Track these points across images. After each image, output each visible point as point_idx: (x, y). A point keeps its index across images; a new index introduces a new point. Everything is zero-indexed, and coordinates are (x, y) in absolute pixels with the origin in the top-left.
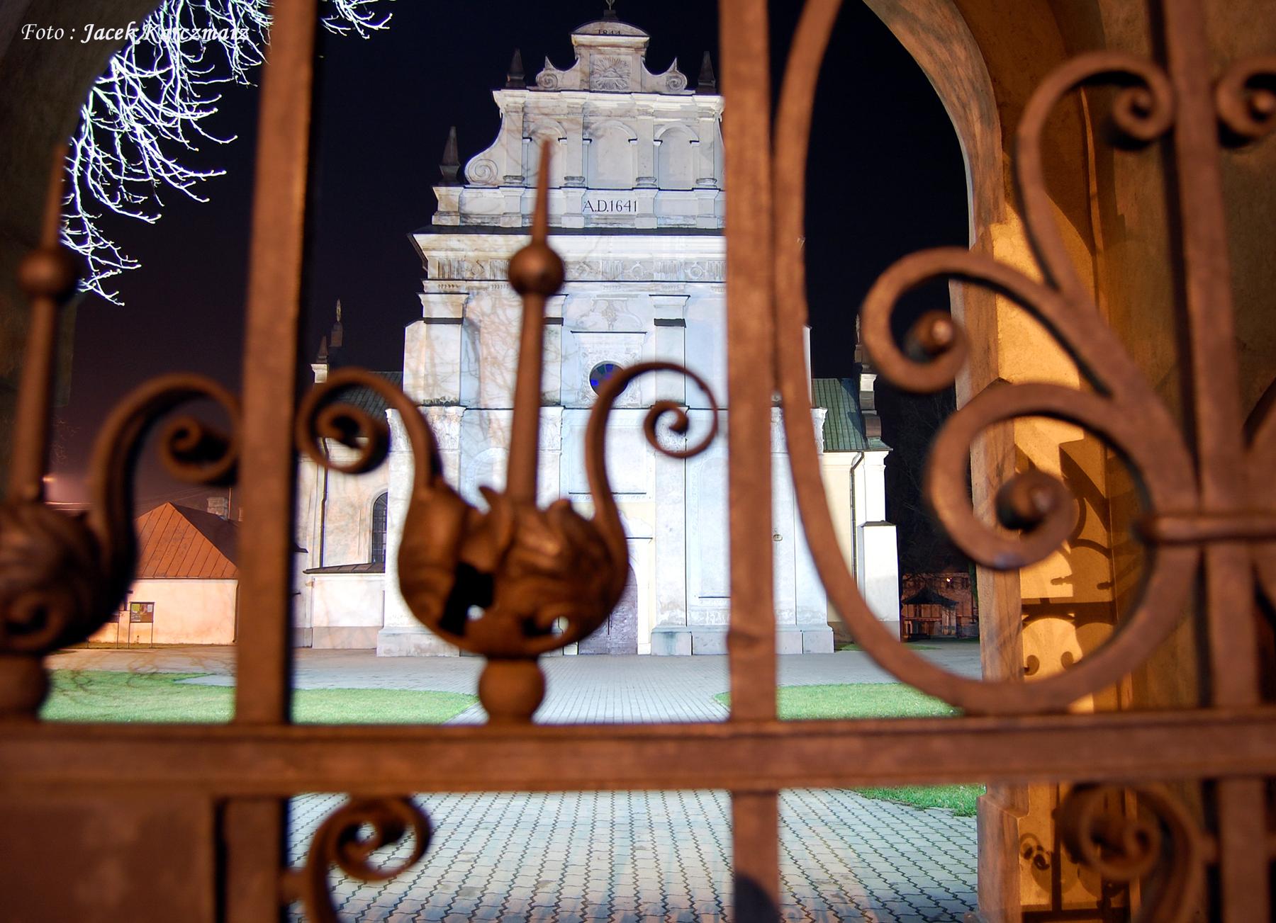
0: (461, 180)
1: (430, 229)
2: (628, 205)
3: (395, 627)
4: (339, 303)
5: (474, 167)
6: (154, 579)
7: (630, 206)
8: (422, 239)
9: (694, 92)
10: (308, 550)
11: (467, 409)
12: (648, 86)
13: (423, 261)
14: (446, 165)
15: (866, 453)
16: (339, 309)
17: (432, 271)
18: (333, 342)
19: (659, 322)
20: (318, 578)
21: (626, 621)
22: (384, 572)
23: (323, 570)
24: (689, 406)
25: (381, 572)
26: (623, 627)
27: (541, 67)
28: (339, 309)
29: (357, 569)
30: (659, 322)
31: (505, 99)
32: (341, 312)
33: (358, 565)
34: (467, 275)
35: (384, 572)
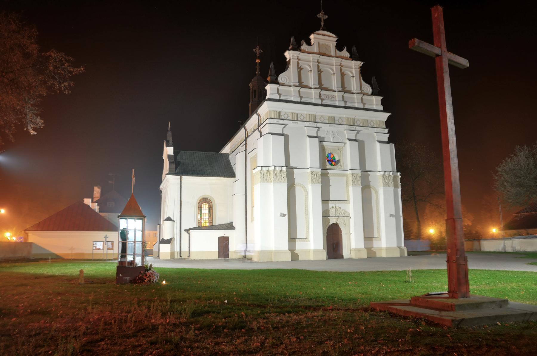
5: (282, 78)
10: (175, 221)
12: (337, 55)
31: (289, 55)
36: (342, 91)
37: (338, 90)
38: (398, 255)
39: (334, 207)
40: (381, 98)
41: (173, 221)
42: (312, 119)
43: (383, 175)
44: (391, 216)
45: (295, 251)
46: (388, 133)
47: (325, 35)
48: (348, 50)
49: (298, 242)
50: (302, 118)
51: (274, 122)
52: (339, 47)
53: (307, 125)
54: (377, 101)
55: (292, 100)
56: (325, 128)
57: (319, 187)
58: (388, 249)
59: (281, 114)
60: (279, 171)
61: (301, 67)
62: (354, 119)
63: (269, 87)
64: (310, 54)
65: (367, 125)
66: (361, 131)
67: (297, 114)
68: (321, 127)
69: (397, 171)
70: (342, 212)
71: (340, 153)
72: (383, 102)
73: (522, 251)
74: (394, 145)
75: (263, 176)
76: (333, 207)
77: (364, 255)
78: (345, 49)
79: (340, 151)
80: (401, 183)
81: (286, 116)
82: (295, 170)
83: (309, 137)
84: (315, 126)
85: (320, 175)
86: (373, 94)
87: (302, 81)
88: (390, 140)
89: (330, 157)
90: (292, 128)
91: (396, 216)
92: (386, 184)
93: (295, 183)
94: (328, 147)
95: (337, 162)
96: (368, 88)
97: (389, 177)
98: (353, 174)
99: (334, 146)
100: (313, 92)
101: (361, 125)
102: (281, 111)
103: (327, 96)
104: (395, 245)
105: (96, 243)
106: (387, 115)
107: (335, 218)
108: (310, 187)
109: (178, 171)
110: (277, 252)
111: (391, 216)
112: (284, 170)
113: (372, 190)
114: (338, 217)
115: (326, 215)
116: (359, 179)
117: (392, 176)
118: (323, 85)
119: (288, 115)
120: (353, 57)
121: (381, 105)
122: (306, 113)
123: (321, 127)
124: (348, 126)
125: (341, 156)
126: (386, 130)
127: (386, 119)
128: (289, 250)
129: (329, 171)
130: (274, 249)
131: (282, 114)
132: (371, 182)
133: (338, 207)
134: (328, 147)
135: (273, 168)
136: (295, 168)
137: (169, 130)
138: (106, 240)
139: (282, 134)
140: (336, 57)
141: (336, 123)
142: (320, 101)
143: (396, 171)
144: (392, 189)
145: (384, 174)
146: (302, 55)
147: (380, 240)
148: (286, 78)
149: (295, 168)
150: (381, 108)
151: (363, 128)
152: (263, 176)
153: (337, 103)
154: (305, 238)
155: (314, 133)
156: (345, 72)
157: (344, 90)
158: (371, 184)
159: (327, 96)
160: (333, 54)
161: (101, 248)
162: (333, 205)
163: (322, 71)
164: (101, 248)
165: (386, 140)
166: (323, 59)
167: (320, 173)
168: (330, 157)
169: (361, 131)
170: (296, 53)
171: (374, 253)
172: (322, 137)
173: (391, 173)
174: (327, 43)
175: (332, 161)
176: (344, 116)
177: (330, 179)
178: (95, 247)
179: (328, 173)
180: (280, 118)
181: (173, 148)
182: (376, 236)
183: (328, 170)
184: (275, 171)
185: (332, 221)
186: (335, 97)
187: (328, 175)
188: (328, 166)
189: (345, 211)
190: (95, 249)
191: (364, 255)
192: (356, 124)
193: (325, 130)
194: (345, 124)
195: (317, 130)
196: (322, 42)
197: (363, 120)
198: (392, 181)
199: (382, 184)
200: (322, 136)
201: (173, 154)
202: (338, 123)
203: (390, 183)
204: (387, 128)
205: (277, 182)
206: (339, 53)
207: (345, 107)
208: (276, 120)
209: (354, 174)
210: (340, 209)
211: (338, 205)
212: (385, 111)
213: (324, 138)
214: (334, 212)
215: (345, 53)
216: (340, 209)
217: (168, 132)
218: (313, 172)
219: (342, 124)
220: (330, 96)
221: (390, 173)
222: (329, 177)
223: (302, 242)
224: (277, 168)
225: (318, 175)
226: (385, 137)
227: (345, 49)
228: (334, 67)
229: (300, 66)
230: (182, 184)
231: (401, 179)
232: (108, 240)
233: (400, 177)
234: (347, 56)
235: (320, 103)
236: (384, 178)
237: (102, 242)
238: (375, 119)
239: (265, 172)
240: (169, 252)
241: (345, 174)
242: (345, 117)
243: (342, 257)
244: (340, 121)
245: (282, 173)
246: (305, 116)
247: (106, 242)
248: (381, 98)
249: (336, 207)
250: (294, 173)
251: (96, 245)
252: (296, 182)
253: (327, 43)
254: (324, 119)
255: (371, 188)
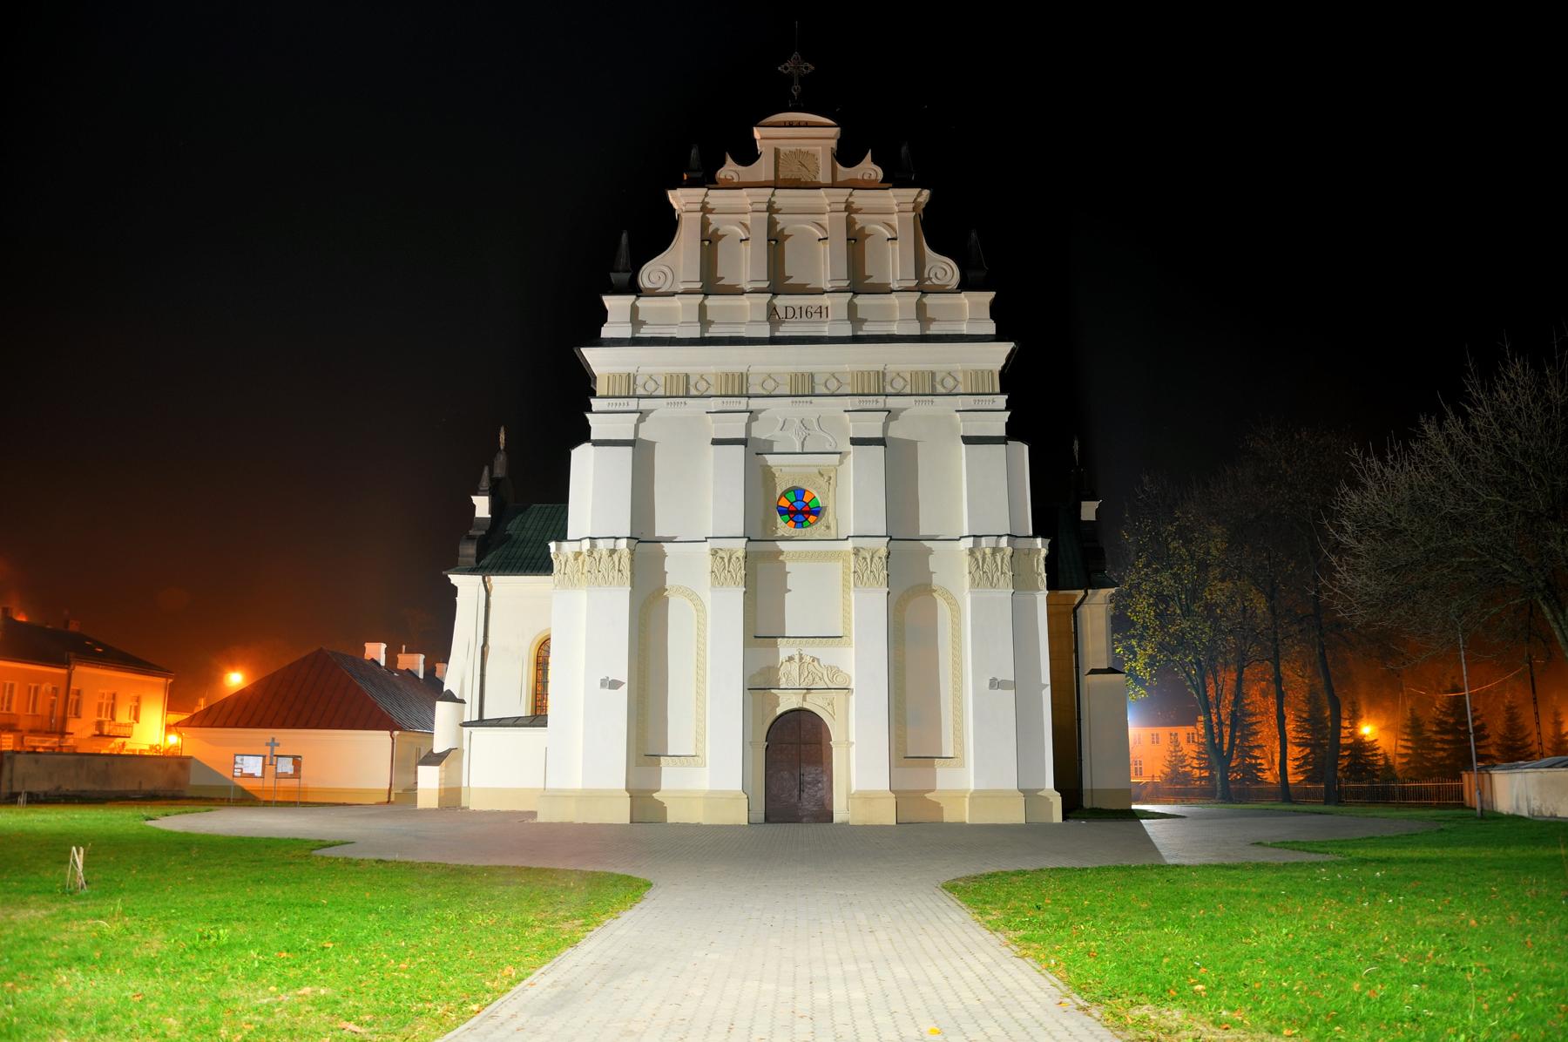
0: (633, 288)
1: (597, 341)
2: (819, 310)
3: (498, 548)
4: (502, 429)
5: (650, 274)
6: (515, 726)
7: (821, 313)
8: (591, 355)
9: (891, 185)
10: (466, 700)
11: (639, 542)
12: (840, 178)
13: (592, 379)
14: (618, 271)
15: (1090, 591)
16: (502, 437)
17: (601, 387)
18: (495, 472)
19: (855, 442)
20: (479, 732)
21: (820, 785)
22: (546, 726)
23: (481, 722)
24: (891, 537)
25: (827, 822)
26: (816, 792)
27: (722, 163)
28: (502, 437)
29: (518, 722)
30: (855, 442)
31: (681, 199)
32: (505, 440)
33: (520, 717)
34: (640, 391)
35: (546, 726)
36: (917, 289)
37: (832, 289)
38: (1019, 817)
39: (797, 658)
40: (991, 295)
41: (462, 701)
42: (869, 387)
43: (970, 549)
44: (995, 684)
45: (654, 795)
46: (1007, 409)
47: (799, 125)
48: (875, 161)
49: (668, 765)
50: (702, 386)
51: (611, 408)
52: (846, 154)
53: (963, 405)
54: (973, 305)
55: (892, 333)
56: (776, 409)
57: (735, 597)
58: (978, 797)
59: (634, 383)
60: (605, 553)
61: (719, 233)
62: (884, 374)
63: (616, 305)
64: (741, 188)
65: (929, 387)
66: (652, 411)
67: (813, 376)
68: (764, 410)
69: (1035, 535)
70: (825, 673)
71: (825, 485)
72: (996, 311)
73: (101, 810)
74: (1026, 448)
75: (563, 569)
76: (791, 659)
77: (620, 813)
78: (869, 155)
79: (826, 478)
80: (1046, 572)
81: (651, 386)
82: (667, 547)
83: (968, 440)
84: (744, 408)
85: (741, 558)
86: (965, 286)
87: (867, 273)
88: (1014, 431)
89: (802, 501)
90: (916, 419)
91: (1020, 685)
92: (982, 576)
93: (667, 586)
94: (783, 468)
95: (817, 512)
96: (944, 269)
97: (993, 554)
98: (858, 551)
99: (803, 466)
100: (897, 302)
101: (908, 390)
102: (635, 372)
103: (798, 312)
104: (1008, 780)
105: (242, 760)
106: (1004, 349)
107: (795, 694)
108: (707, 595)
109: (484, 562)
110: (587, 796)
111: (995, 684)
112: (621, 548)
113: (938, 600)
114: (805, 691)
115: (759, 685)
116: (879, 565)
117: (1009, 551)
118: (723, 278)
119: (707, 382)
120: (894, 178)
121: (991, 317)
122: (714, 371)
123: (764, 410)
124: (857, 399)
125: (830, 494)
126: (1002, 400)
127: (1003, 362)
128: (627, 790)
129: (782, 545)
130: (580, 787)
131: (640, 381)
132: (934, 575)
133: (808, 659)
134: (783, 468)
135: (586, 544)
136: (671, 540)
137: (502, 447)
138: (272, 751)
139: (884, 439)
140: (834, 185)
141: (817, 392)
142: (917, 325)
143: (1031, 533)
144: (1004, 593)
145: (976, 545)
146: (717, 198)
147: (962, 765)
148: (944, 269)
149: (671, 540)
150: (990, 328)
151: (913, 398)
152: (563, 569)
153: (895, 328)
154: (694, 754)
155: (872, 426)
156: (867, 228)
157: (859, 283)
158: (936, 581)
159: (798, 312)
160: (824, 176)
161: (258, 773)
162: (794, 652)
163: (870, 235)
164: (258, 773)
165: (1002, 432)
166: (784, 198)
167: (741, 554)
168: (802, 501)
169: (652, 411)
170: (698, 193)
171: (661, 808)
172: (765, 440)
173: (1004, 542)
174: (804, 149)
175: (802, 512)
176: (847, 368)
177: (787, 570)
178: (242, 769)
179: (781, 552)
180: (631, 394)
181: (487, 498)
182: (948, 751)
183: (777, 542)
184: (595, 554)
185: (788, 702)
186: (824, 311)
187: (781, 558)
188: (783, 526)
189: (835, 671)
190: (239, 774)
191: (620, 813)
192: (889, 390)
193: (778, 417)
194: (850, 392)
195: (635, 422)
196: (785, 147)
197: (916, 373)
198: (1006, 569)
199: (967, 579)
200: (763, 438)
201: (490, 516)
202: (826, 391)
203: (999, 573)
204: (1002, 392)
205: (599, 586)
206: (844, 173)
207: (856, 339)
208: (734, 399)
209: (720, 552)
210: (816, 663)
211: (810, 651)
212: (999, 337)
213: (771, 443)
214: (795, 673)
215: (868, 169)
216: (816, 663)
217: (498, 455)
218: (716, 552)
219: (839, 392)
220: (806, 312)
221: (997, 542)
222: (783, 563)
223: (683, 765)
224: (601, 544)
225: (734, 558)
226: (997, 424)
227: (869, 155)
228: (895, 217)
229: (710, 230)
230: (491, 598)
231: (1047, 559)
232: (277, 751)
233: (1044, 552)
234: (873, 177)
235: (767, 335)
236: (977, 560)
237: (261, 758)
238: (959, 366)
239: (569, 556)
240: (437, 787)
241: (770, 552)
242: (848, 370)
243: (825, 815)
244: (833, 386)
245: (616, 557)
246: (712, 382)
247: (271, 758)
248: (991, 295)
249: (801, 658)
250: (664, 555)
251: (242, 764)
252: (667, 586)
253: (805, 146)
254: (778, 384)
255: (935, 595)
